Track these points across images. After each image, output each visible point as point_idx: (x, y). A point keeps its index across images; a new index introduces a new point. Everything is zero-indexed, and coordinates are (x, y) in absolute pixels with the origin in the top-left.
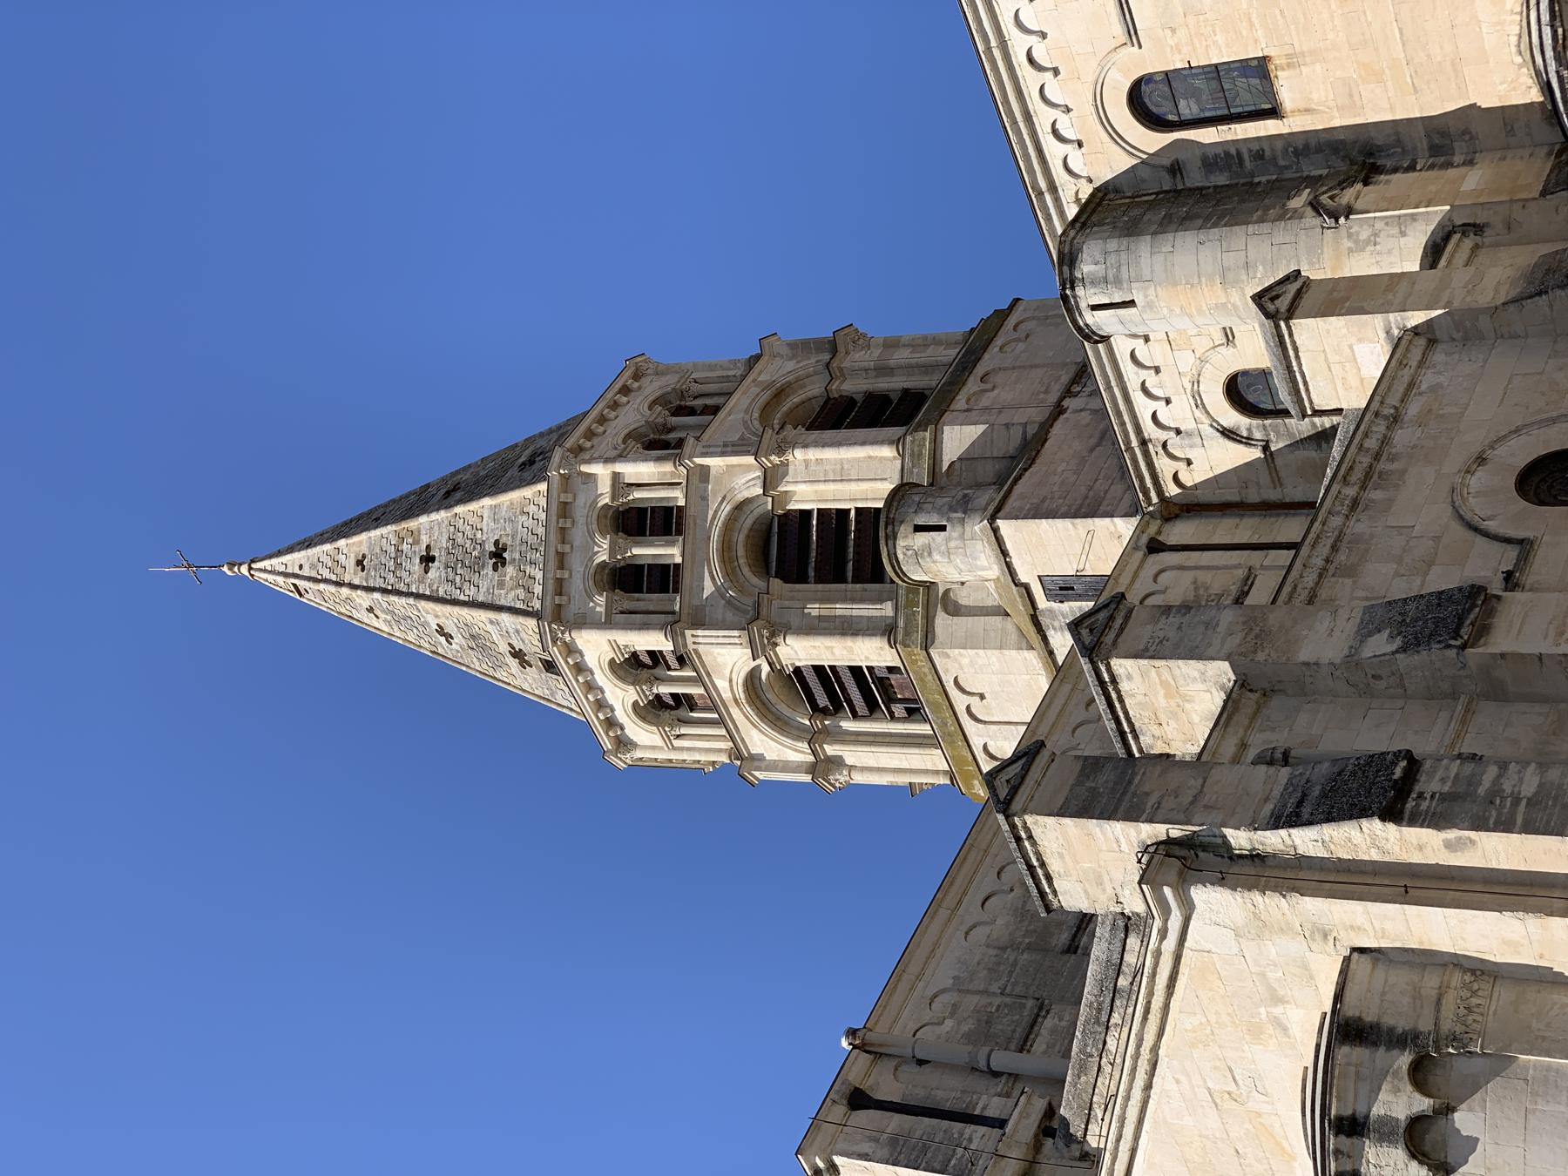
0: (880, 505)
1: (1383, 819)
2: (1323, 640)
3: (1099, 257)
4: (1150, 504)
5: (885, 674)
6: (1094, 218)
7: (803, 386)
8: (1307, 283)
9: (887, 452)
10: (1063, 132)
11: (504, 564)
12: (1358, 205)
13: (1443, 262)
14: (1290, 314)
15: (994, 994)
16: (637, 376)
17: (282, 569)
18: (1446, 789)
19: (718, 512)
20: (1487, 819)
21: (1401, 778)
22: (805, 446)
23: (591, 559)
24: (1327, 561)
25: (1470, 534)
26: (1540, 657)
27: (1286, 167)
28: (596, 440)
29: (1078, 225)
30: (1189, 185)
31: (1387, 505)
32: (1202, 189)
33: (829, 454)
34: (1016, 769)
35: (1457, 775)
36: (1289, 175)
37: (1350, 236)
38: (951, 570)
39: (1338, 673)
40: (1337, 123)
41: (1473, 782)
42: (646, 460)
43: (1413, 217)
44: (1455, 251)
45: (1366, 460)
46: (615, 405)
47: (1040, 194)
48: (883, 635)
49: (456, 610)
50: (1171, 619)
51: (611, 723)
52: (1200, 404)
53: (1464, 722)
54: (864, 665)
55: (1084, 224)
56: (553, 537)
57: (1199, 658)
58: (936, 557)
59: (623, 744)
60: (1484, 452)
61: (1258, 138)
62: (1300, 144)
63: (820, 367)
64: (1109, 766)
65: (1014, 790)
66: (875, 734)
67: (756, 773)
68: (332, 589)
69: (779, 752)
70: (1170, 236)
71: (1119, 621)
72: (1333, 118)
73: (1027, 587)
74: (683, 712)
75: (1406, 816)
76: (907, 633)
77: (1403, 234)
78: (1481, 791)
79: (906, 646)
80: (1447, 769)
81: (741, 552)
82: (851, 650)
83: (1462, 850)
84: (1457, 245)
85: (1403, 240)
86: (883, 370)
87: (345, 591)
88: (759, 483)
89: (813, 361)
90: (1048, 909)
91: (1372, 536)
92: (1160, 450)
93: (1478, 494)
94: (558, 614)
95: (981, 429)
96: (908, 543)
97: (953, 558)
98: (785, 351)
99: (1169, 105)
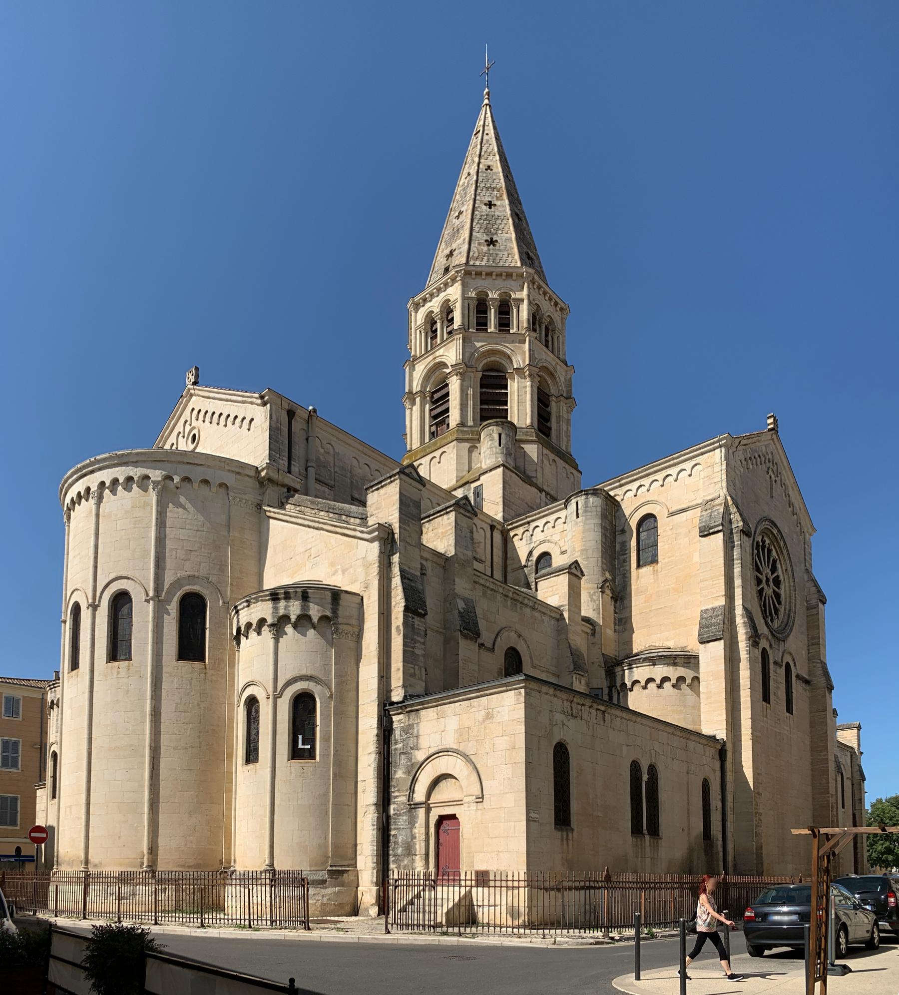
2: (462, 586)
8: (580, 579)
9: (528, 422)
12: (605, 595)
16: (562, 309)
19: (507, 348)
33: (528, 396)
34: (415, 476)
36: (617, 571)
40: (633, 587)
41: (418, 634)
45: (520, 600)
47: (619, 481)
51: (425, 300)
53: (437, 632)
58: (490, 443)
59: (417, 306)
68: (478, 153)
73: (479, 479)
74: (430, 334)
76: (462, 431)
81: (492, 359)
82: (455, 408)
86: (559, 418)
90: (367, 489)
94: (469, 274)
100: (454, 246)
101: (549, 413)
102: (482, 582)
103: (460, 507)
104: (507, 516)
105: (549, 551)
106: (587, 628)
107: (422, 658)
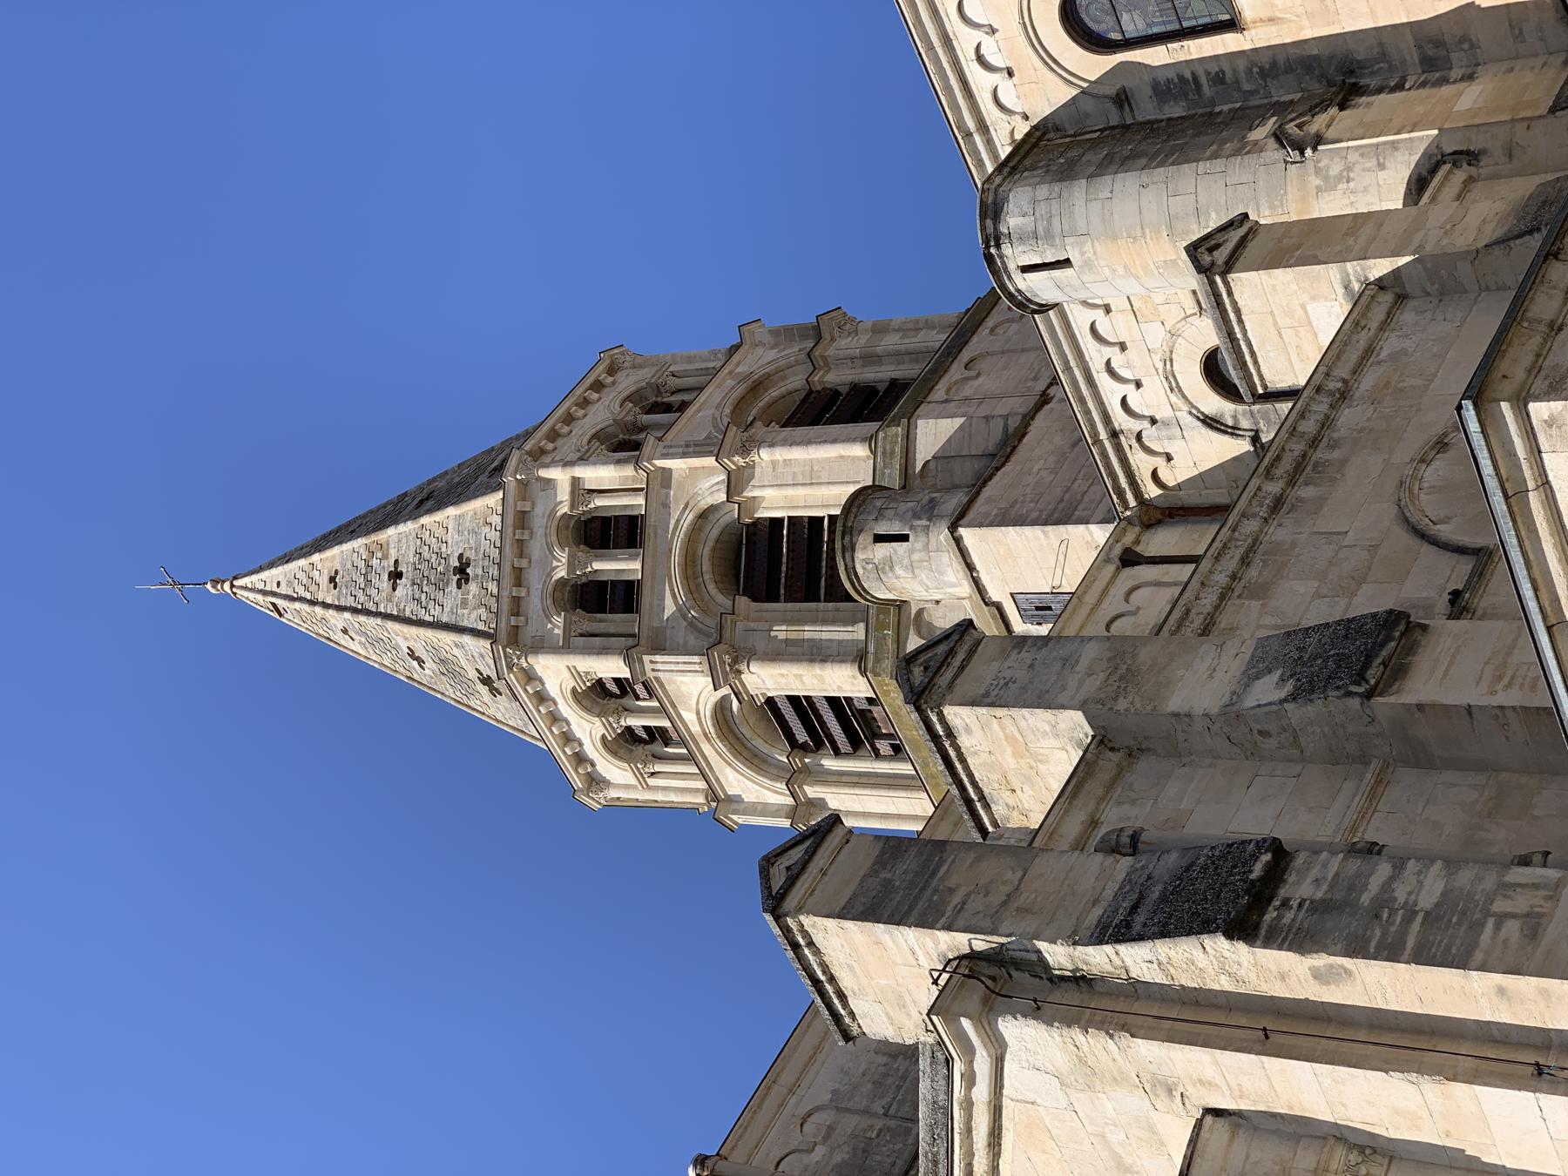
0: (837, 512)
1: (1230, 936)
2: (1201, 684)
3: (1027, 208)
4: (1127, 507)
5: (865, 706)
6: (1027, 162)
7: (784, 378)
8: (1255, 229)
9: (860, 451)
10: (990, 59)
11: (467, 581)
12: (1329, 134)
13: (1425, 199)
14: (1229, 267)
15: (875, 1115)
16: (612, 370)
17: (261, 586)
18: (1319, 895)
19: (680, 521)
20: (1368, 941)
21: (1260, 879)
22: (772, 445)
23: (549, 575)
24: (1233, 577)
25: (1415, 542)
26: (1469, 710)
27: (1252, 93)
28: (560, 442)
29: (1006, 170)
30: (1140, 119)
31: (1321, 501)
32: (1151, 122)
33: (797, 454)
34: (796, 854)
35: (1337, 874)
36: (1255, 101)
37: (1318, 171)
38: (917, 587)
39: (1214, 728)
40: (1308, 33)
41: (1356, 884)
42: (605, 463)
43: (1394, 146)
44: (1442, 185)
45: (1298, 447)
46: (585, 403)
47: (969, 135)
48: (853, 661)
49: (421, 631)
50: (1023, 654)
51: (580, 759)
52: (1175, 387)
53: (1373, 796)
54: (841, 695)
55: (1014, 169)
56: (508, 551)
57: (1048, 706)
58: (899, 571)
59: (595, 782)
60: (1445, 435)
61: (1216, 57)
62: (1265, 61)
63: (803, 356)
64: (914, 851)
65: (791, 882)
66: (860, 774)
67: (734, 817)
68: (306, 607)
69: (759, 796)
70: (1108, 179)
71: (960, 657)
72: (1302, 28)
73: (999, 607)
74: (658, 747)
75: (1263, 932)
76: (877, 660)
77: (1382, 167)
78: (1365, 899)
79: (876, 675)
80: (1325, 865)
81: (706, 566)
82: (821, 679)
83: (1336, 983)
84: (1446, 178)
85: (1382, 175)
86: (869, 358)
87: (318, 609)
88: (724, 487)
89: (796, 349)
90: (847, 1036)
91: (1294, 545)
92: (1136, 445)
93: (1433, 489)
94: (512, 636)
95: (958, 422)
96: (868, 555)
97: (921, 576)
98: (767, 339)
99: (1110, 20)
100: (473, 675)
101: (855, 388)
102: (1209, 600)
103: (929, 685)
104: (1101, 511)
105: (1199, 355)
106: (1450, 181)
107: (1464, 877)
